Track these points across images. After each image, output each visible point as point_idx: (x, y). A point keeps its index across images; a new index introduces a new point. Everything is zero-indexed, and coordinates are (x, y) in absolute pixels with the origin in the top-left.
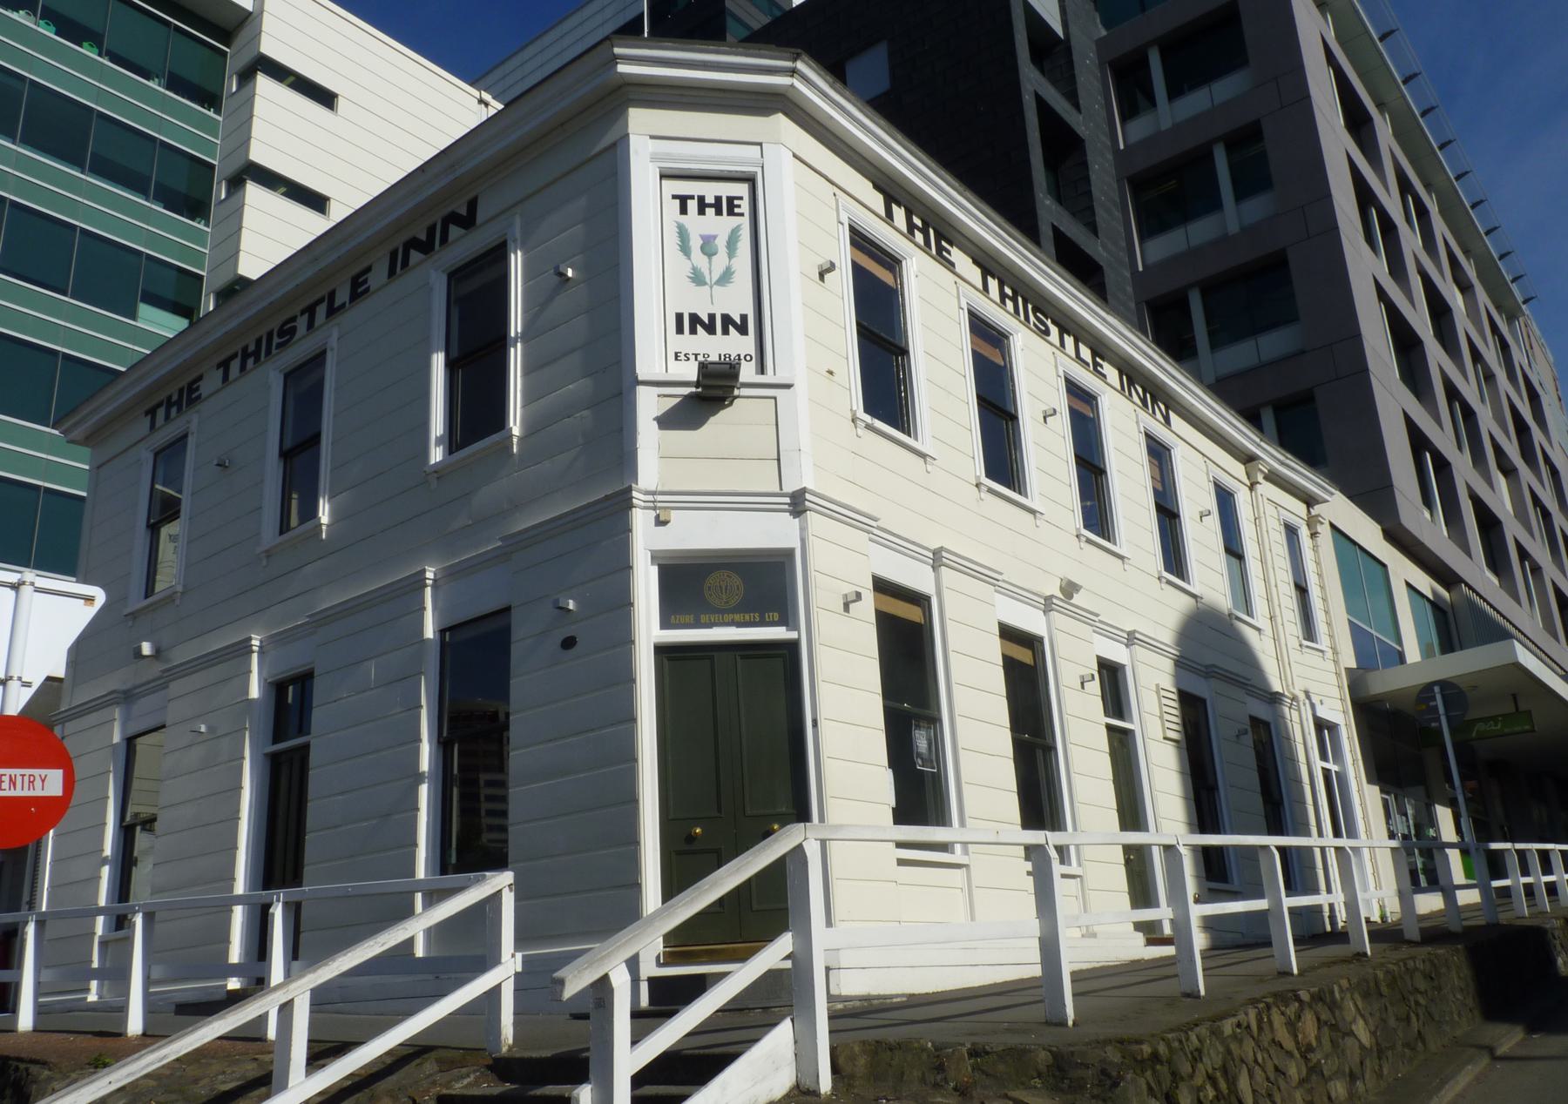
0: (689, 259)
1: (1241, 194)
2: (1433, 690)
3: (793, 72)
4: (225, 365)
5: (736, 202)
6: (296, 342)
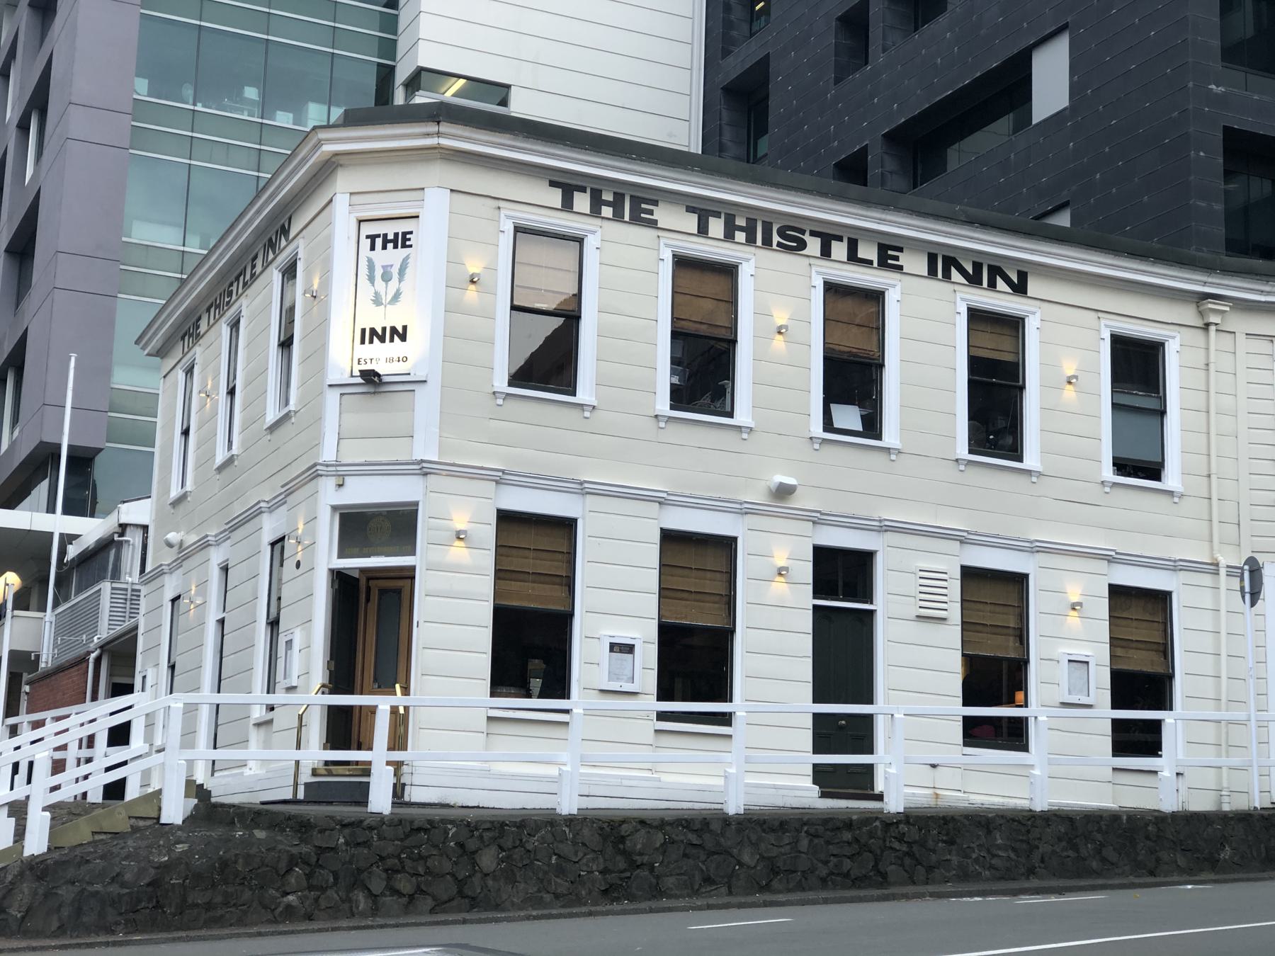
0: (373, 286)
5: (408, 236)
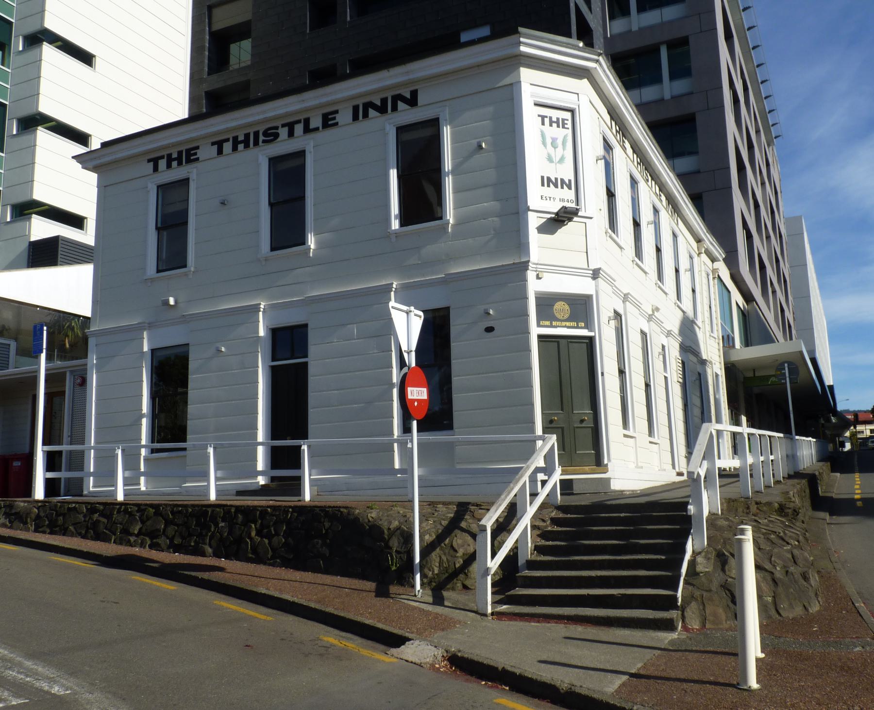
1: (673, 76)
2: (784, 366)
3: (597, 61)
4: (219, 145)
5: (566, 122)
6: (278, 142)
